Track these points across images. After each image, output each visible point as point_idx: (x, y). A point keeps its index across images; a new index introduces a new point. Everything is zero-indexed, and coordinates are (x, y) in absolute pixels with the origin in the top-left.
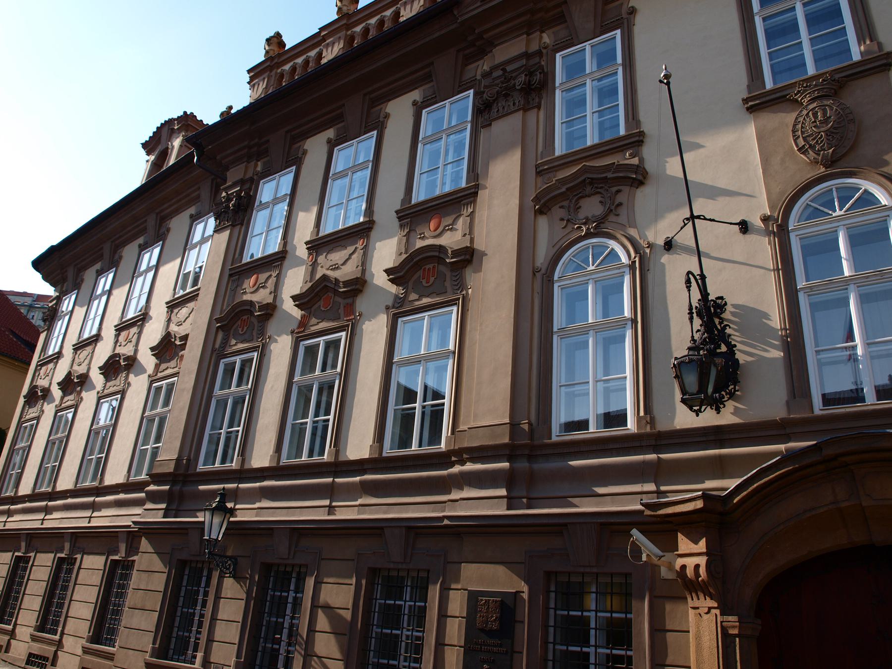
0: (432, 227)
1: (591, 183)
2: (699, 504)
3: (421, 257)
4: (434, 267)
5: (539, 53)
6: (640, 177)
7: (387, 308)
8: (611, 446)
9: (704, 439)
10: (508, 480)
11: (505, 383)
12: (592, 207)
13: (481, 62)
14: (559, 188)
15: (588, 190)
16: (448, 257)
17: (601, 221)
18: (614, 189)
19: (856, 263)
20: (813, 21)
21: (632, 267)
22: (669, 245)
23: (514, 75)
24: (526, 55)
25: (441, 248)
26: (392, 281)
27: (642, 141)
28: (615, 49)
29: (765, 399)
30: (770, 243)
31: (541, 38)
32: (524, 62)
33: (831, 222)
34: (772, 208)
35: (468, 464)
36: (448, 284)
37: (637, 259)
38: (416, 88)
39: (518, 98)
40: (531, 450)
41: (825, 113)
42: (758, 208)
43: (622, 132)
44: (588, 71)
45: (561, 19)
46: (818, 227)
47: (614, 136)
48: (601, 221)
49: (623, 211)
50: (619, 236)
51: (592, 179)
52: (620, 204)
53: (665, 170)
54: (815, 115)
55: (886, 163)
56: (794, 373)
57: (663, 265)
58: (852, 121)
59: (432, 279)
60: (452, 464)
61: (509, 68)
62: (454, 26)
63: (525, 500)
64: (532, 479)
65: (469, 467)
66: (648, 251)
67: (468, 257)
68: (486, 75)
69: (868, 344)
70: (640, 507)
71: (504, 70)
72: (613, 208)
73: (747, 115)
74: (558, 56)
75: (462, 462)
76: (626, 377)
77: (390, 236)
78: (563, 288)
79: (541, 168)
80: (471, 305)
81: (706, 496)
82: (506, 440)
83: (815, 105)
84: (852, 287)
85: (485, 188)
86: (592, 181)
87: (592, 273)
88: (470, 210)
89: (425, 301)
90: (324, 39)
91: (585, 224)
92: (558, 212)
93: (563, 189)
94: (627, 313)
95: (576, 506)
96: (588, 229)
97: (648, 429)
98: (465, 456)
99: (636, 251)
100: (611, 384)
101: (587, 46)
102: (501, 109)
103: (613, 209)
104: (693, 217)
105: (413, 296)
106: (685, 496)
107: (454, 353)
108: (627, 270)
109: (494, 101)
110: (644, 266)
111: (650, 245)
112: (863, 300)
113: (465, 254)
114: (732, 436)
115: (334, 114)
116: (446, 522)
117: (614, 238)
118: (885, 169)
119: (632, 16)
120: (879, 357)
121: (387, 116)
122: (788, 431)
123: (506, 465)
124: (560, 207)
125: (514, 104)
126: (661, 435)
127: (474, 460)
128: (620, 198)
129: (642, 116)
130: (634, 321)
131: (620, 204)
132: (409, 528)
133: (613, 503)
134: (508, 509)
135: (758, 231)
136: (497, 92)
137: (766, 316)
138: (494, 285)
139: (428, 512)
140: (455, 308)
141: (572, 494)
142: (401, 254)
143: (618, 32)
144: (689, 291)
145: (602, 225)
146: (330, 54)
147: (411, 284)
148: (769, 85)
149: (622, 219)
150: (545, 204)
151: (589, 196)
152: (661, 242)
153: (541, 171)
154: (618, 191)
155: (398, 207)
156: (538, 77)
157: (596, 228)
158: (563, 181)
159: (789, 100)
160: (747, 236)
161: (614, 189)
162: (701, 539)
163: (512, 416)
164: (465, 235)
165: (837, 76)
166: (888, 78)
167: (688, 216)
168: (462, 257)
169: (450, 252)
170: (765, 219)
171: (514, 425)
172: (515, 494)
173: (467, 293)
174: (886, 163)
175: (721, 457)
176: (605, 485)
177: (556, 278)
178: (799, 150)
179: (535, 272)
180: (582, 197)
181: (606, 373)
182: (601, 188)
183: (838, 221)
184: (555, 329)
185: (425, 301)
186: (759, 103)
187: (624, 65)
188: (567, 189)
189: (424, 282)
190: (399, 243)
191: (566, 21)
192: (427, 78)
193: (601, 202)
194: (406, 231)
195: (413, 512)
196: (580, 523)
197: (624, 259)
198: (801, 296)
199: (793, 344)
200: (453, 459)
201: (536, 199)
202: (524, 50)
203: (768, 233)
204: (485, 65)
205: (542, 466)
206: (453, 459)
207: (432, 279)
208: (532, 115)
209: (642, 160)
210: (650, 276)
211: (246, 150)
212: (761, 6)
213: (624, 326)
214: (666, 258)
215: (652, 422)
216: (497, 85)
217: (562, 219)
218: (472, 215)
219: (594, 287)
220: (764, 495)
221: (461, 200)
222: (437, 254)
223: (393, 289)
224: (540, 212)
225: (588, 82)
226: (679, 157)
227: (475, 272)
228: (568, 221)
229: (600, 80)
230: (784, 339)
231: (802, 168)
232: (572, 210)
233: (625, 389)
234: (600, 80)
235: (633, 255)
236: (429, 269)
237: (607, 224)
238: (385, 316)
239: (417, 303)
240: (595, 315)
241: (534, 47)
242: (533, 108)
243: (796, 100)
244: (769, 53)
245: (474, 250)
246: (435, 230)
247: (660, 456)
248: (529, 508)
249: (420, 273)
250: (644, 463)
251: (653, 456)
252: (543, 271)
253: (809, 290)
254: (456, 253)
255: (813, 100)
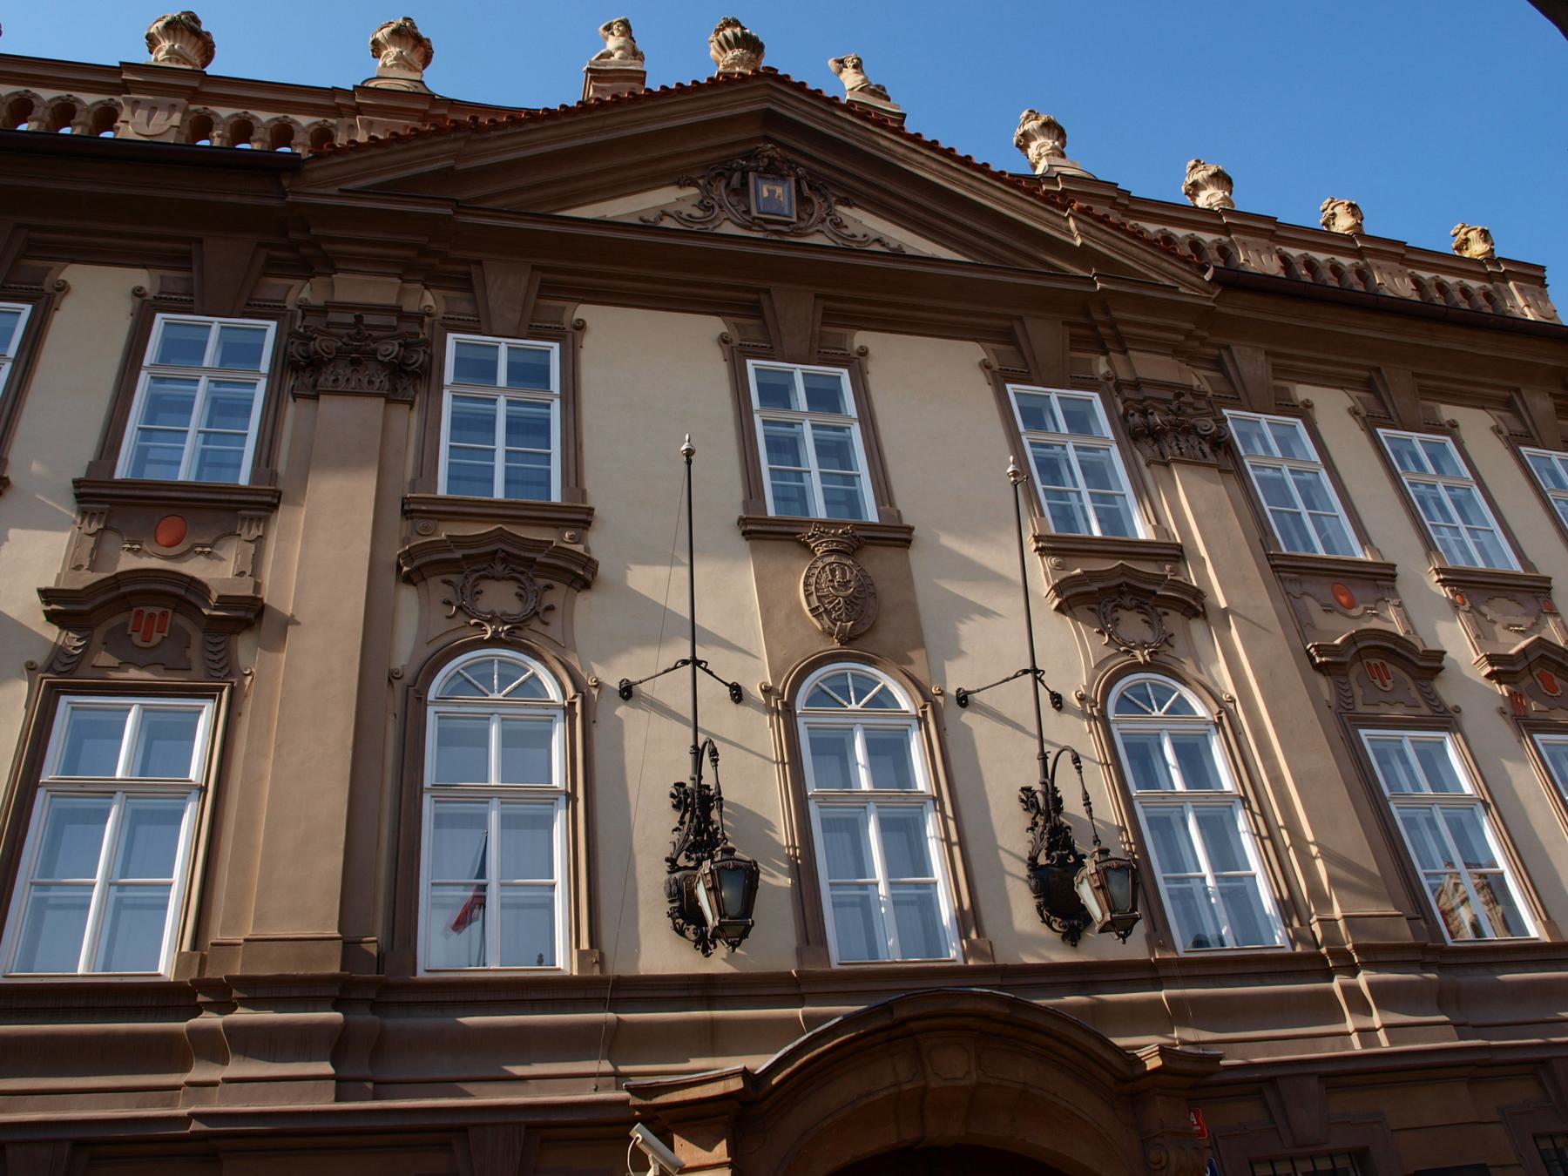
0: (163, 538)
1: (503, 560)
2: (736, 1084)
3: (138, 587)
4: (164, 614)
5: (419, 318)
6: (589, 577)
7: (31, 668)
8: (533, 996)
9: (685, 993)
10: (336, 1045)
11: (334, 863)
12: (500, 597)
13: (298, 283)
14: (450, 551)
15: (499, 568)
16: (208, 606)
17: (518, 625)
18: (542, 582)
19: (875, 780)
20: (513, 426)
21: (569, 710)
22: (627, 691)
23: (375, 334)
24: (396, 311)
25: (196, 586)
26: (51, 617)
27: (589, 523)
28: (12, 330)
29: (772, 946)
30: (772, 725)
31: (422, 296)
32: (394, 321)
33: (847, 716)
34: (775, 677)
35: (240, 1010)
36: (194, 654)
37: (578, 701)
38: (144, 267)
39: (382, 380)
40: (372, 992)
41: (843, 575)
42: (758, 676)
43: (244, 479)
44: (207, 363)
45: (464, 283)
46: (827, 718)
47: (171, 479)
48: (518, 625)
49: (555, 619)
50: (548, 657)
51: (508, 554)
52: (551, 608)
53: (625, 578)
54: (833, 571)
55: (910, 662)
56: (807, 910)
57: (620, 720)
58: (874, 595)
59: (156, 638)
60: (197, 1011)
61: (369, 319)
62: (274, 203)
63: (370, 1085)
64: (380, 1046)
65: (243, 1015)
66: (595, 692)
67: (251, 615)
68: (307, 309)
69: (502, 885)
70: (625, 1095)
71: (359, 319)
72: (540, 610)
73: (744, 545)
74: (159, 317)
75: (226, 1007)
76: (170, 885)
77: (49, 523)
78: (442, 717)
79: (413, 506)
80: (248, 707)
81: (745, 1074)
82: (335, 969)
83: (832, 559)
84: (495, 802)
85: (297, 502)
86: (508, 558)
87: (497, 704)
88: (255, 533)
89: (133, 674)
90: (358, 110)
91: (490, 622)
92: (438, 589)
93: (458, 554)
94: (558, 779)
95: (468, 1095)
96: (495, 632)
97: (596, 972)
98: (235, 994)
99: (577, 688)
100: (128, 893)
101: (216, 323)
102: (342, 380)
103: (541, 613)
104: (695, 662)
105: (104, 659)
106: (720, 1072)
107: (203, 790)
108: (560, 714)
109: (330, 360)
110: (586, 709)
111: (598, 685)
112: (506, 822)
113: (247, 610)
114: (726, 992)
115: (1140, 331)
116: (196, 1126)
117: (538, 657)
118: (907, 667)
119: (59, 294)
120: (518, 906)
121: (63, 288)
122: (803, 990)
123: (336, 1016)
124: (445, 582)
125: (370, 382)
126: (622, 983)
127: (253, 1003)
128: (549, 598)
129: (589, 483)
130: (571, 797)
131: (551, 608)
132: (78, 1144)
133: (540, 1091)
134: (337, 1100)
135: (755, 704)
136: (338, 349)
137: (770, 826)
138: (309, 684)
139: (96, 1108)
140: (208, 707)
141: (465, 1075)
142: (78, 568)
143: (27, 309)
144: (1079, 768)
145: (518, 632)
146: (133, 126)
147: (99, 634)
148: (442, 491)
149: (554, 631)
150: (418, 569)
151: (498, 579)
152: (614, 682)
153: (412, 511)
154: (549, 587)
155: (81, 474)
156: (419, 358)
157: (509, 632)
158: (457, 541)
159: (798, 541)
160: (740, 707)
161: (548, 582)
162: (717, 1142)
163: (342, 927)
164: (241, 574)
165: (858, 533)
166: (907, 558)
167: (688, 657)
168: (241, 614)
169: (214, 596)
170: (767, 691)
171: (350, 946)
172: (347, 1072)
173: (241, 683)
174: (910, 662)
175: (713, 1023)
176: (528, 1063)
177: (431, 696)
178: (812, 610)
179: (393, 677)
180: (486, 577)
181: (124, 875)
182: (522, 573)
183: (856, 717)
184: (427, 783)
185: (133, 674)
186: (759, 531)
187: (563, 398)
188: (465, 557)
189: (137, 638)
190: (75, 546)
191: (190, 269)
192: (180, 260)
193: (519, 596)
194: (95, 527)
195: (82, 1108)
196: (492, 1125)
197: (554, 694)
198: (41, 795)
199: (803, 871)
200: (201, 998)
201: (408, 556)
202: (393, 302)
203: (772, 711)
204: (307, 292)
205: (397, 1022)
206: (201, 998)
207: (156, 638)
208: (399, 412)
209: (587, 549)
210: (598, 733)
211: (1181, 338)
212: (222, 363)
213: (184, 797)
214: (622, 710)
215: (601, 961)
216: (340, 337)
217: (449, 603)
218: (260, 541)
219: (501, 728)
220: (810, 1075)
221: (247, 508)
222: (182, 592)
223: (52, 633)
224: (408, 579)
225: (203, 381)
226: (685, 571)
227: (266, 648)
228: (459, 608)
229: (218, 383)
230: (791, 860)
231: (811, 635)
232: (467, 592)
233: (165, 907)
234: (218, 383)
235: (571, 692)
236: (151, 616)
237: (526, 633)
238: (25, 685)
239: (114, 675)
240: (129, 766)
241: (411, 305)
242: (404, 402)
243: (807, 545)
244: (507, 452)
245: (263, 607)
246: (169, 546)
247: (622, 1016)
248: (375, 1098)
249: (130, 617)
250: (594, 1027)
251: (611, 1016)
252: (407, 679)
253: (56, 790)
254: (224, 601)
255: (831, 552)
